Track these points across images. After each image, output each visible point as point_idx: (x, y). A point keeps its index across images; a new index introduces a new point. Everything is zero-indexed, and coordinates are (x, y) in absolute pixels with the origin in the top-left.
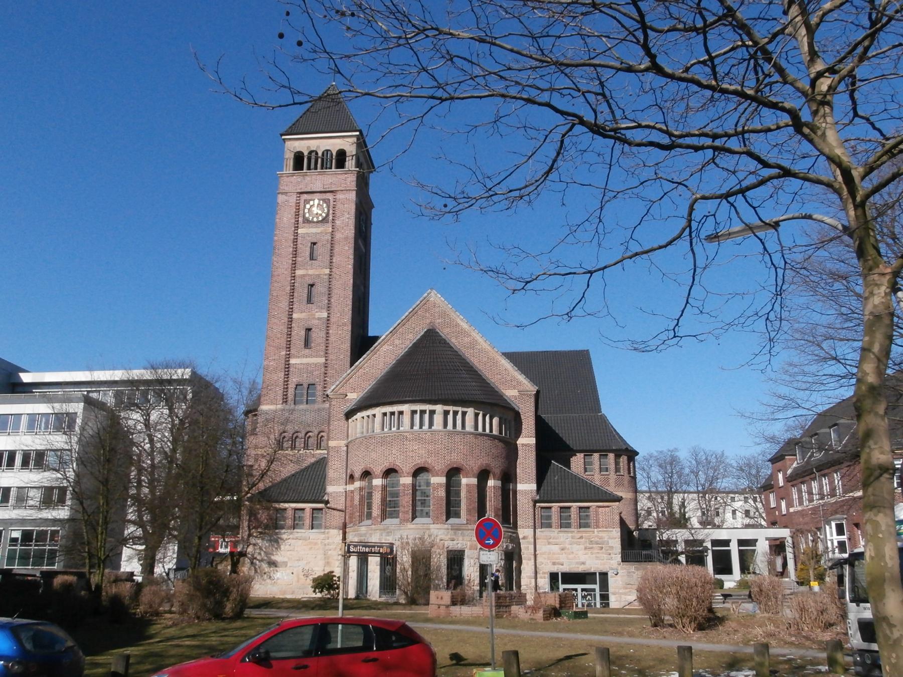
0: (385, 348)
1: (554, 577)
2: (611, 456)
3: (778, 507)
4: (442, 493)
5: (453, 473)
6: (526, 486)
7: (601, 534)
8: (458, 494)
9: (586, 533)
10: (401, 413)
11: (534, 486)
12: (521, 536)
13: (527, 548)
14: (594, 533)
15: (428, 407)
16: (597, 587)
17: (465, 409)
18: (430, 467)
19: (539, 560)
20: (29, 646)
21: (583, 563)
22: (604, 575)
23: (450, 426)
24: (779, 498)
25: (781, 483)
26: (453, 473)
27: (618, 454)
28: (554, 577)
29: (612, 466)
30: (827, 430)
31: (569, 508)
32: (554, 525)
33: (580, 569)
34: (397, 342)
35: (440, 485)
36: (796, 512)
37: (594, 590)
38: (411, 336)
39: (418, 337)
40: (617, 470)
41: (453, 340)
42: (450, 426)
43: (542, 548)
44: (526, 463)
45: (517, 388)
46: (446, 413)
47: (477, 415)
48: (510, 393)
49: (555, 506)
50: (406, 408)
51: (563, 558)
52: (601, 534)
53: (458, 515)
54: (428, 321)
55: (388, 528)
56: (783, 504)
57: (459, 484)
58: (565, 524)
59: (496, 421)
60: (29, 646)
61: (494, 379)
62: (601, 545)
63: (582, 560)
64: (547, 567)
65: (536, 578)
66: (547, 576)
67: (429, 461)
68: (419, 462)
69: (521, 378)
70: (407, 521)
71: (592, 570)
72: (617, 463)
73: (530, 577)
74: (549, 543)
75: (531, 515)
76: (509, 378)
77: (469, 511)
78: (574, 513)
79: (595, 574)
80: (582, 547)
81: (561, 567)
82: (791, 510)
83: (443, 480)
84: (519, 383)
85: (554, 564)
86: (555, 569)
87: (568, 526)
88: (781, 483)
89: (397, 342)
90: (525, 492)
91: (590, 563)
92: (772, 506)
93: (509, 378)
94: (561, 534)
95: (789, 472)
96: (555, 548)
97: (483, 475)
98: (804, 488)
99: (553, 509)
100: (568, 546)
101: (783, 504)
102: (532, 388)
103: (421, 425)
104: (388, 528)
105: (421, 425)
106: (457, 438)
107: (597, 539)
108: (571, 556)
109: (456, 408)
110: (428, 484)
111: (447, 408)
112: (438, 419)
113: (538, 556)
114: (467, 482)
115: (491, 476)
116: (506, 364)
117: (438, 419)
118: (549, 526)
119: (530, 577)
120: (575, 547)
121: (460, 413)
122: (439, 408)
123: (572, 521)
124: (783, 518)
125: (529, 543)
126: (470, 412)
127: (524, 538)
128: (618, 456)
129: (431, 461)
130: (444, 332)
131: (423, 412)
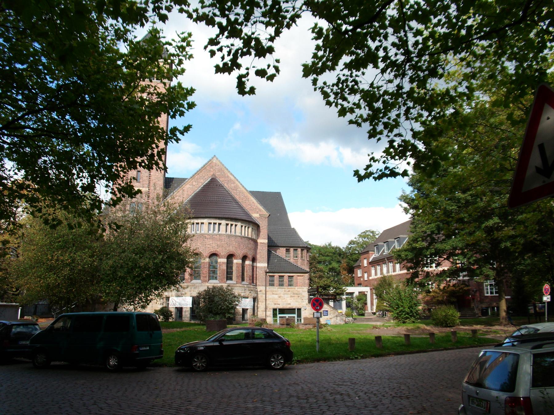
0: (188, 186)
1: (275, 310)
2: (299, 250)
3: (363, 277)
4: (224, 267)
5: (230, 257)
6: (262, 265)
7: (298, 290)
8: (231, 268)
9: (292, 289)
10: (202, 223)
11: (266, 265)
12: (259, 290)
13: (262, 296)
14: (296, 289)
15: (218, 221)
16: (296, 315)
17: (236, 224)
18: (218, 254)
19: (268, 302)
20: (503, 245)
21: (290, 304)
22: (299, 310)
23: (229, 232)
24: (364, 272)
25: (365, 265)
26: (230, 257)
27: (303, 249)
28: (275, 310)
29: (300, 255)
30: (393, 240)
31: (283, 276)
32: (275, 285)
33: (288, 307)
34: (194, 183)
35: (223, 263)
36: (373, 279)
37: (294, 317)
38: (202, 181)
39: (206, 182)
40: (302, 257)
41: (226, 185)
42: (229, 232)
43: (269, 296)
44: (262, 252)
45: (258, 212)
46: (227, 225)
47: (242, 226)
48: (255, 216)
49: (277, 275)
50: (206, 221)
51: (280, 301)
52: (298, 290)
53: (231, 279)
54: (212, 173)
55: (194, 285)
56: (366, 275)
57: (232, 263)
58: (281, 285)
59: (250, 229)
60: (503, 245)
61: (247, 207)
62: (298, 295)
63: (289, 302)
64: (271, 306)
65: (266, 311)
66: (272, 310)
67: (218, 250)
68: (213, 251)
69: (261, 208)
70: (205, 281)
71: (294, 307)
72: (302, 254)
73: (263, 311)
74: (273, 294)
75: (264, 279)
76: (255, 207)
77: (237, 277)
78: (286, 279)
79: (295, 309)
82: (370, 278)
83: (225, 260)
84: (260, 210)
85: (275, 304)
86: (275, 307)
87: (282, 285)
88: (365, 265)
89: (194, 183)
90: (261, 268)
91: (293, 304)
92: (359, 276)
93: (255, 207)
95: (371, 260)
96: (276, 296)
97: (244, 258)
98: (378, 268)
99: (275, 277)
100: (282, 295)
101: (366, 275)
102: (267, 214)
103: (214, 230)
104: (194, 285)
105: (214, 230)
106: (233, 239)
108: (284, 301)
109: (232, 223)
110: (216, 262)
111: (227, 222)
112: (223, 227)
113: (267, 301)
114: (237, 261)
115: (248, 259)
116: (253, 199)
117: (223, 227)
118: (273, 285)
119: (263, 311)
120: (286, 296)
121: (234, 226)
122: (224, 222)
123: (285, 282)
124: (366, 282)
125: (263, 293)
126: (239, 224)
127: (260, 291)
128: (302, 250)
129: (219, 250)
130: (221, 180)
131: (215, 224)
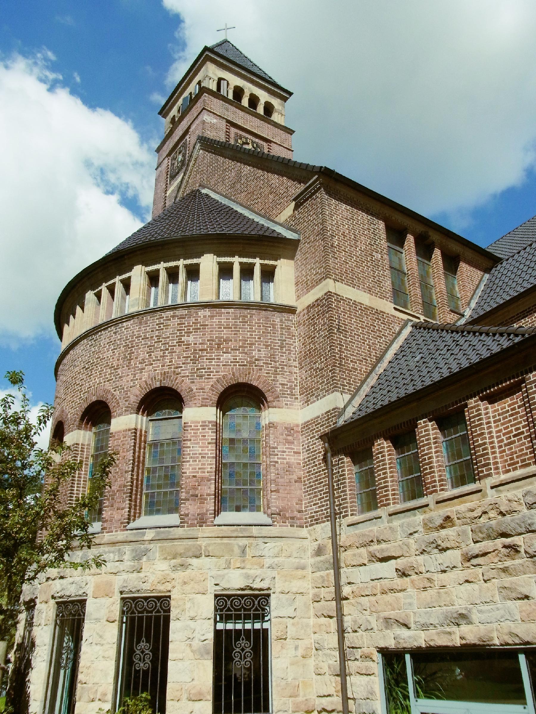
63: (460, 606)
80: (454, 556)
81: (404, 633)
94: (397, 522)
107: (494, 521)
